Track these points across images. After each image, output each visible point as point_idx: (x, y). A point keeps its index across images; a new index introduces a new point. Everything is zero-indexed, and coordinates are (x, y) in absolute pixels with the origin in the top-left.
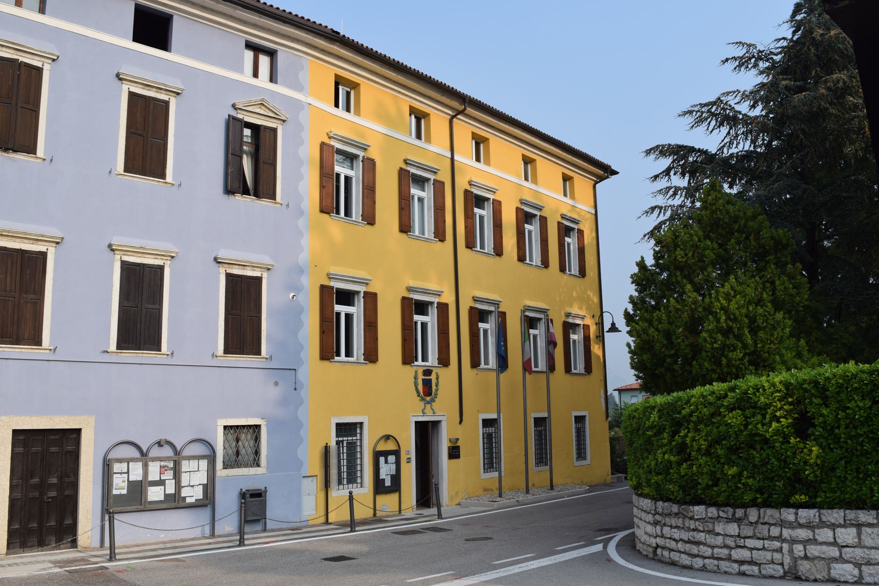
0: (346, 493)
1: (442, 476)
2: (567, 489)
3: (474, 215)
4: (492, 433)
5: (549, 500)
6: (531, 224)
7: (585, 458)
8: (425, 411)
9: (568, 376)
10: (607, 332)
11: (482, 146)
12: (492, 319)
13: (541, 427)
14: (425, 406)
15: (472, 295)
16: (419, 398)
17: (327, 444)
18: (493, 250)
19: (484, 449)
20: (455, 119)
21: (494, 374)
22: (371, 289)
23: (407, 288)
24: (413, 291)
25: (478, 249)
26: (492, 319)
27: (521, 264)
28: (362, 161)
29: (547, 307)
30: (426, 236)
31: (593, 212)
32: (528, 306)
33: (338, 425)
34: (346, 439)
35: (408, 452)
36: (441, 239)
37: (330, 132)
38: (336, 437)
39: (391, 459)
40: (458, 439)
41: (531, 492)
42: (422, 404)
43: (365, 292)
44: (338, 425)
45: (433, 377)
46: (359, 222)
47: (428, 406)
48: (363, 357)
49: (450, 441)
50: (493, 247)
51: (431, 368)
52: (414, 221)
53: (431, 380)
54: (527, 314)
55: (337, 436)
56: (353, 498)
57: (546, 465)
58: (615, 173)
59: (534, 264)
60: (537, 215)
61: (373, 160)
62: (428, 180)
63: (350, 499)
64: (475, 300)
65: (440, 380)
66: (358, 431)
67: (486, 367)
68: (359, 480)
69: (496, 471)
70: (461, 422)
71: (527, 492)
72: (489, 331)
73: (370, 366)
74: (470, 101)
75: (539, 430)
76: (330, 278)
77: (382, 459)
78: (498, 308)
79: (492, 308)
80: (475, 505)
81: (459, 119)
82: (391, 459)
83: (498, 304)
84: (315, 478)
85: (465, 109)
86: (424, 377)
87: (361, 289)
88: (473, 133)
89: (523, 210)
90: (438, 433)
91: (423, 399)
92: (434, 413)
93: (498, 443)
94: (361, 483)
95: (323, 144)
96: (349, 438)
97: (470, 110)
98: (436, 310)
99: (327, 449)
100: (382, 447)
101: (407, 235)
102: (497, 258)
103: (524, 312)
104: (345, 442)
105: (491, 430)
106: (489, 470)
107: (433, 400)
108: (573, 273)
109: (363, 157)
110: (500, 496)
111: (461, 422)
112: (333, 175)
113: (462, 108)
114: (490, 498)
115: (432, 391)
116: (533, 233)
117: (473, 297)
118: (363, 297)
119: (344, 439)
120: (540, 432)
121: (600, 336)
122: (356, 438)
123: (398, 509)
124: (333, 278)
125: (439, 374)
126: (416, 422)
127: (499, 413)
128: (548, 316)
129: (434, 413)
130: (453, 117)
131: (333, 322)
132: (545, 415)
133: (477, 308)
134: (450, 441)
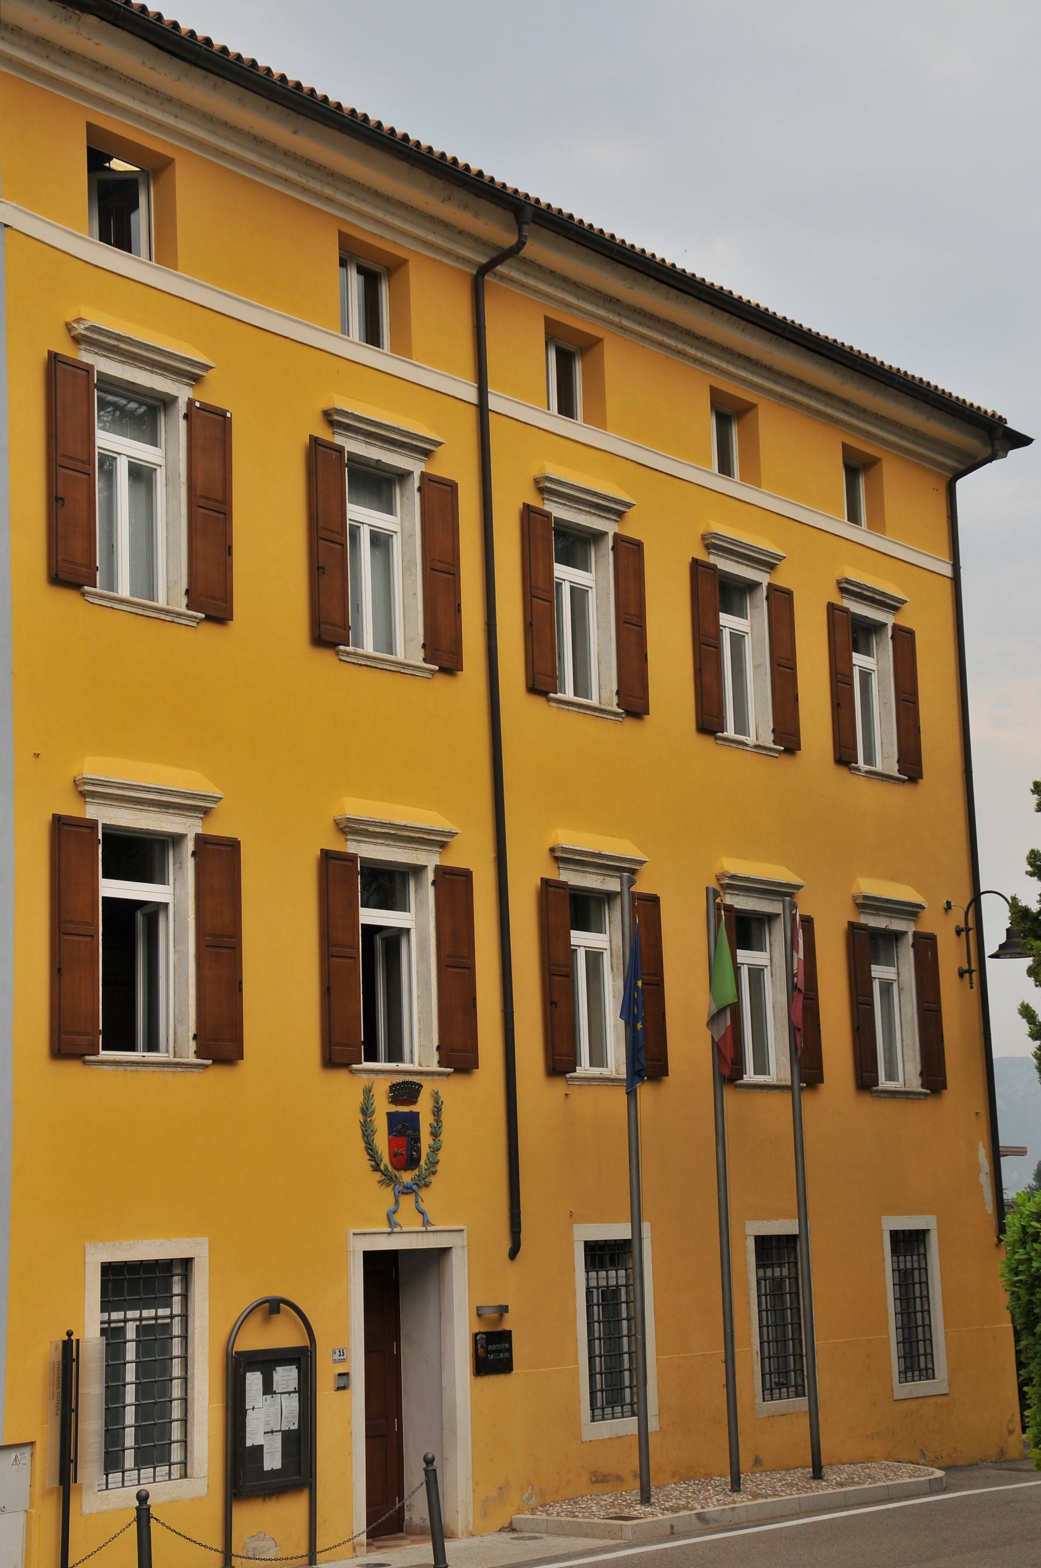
0: (124, 1499)
1: (454, 1432)
2: (870, 1476)
3: (553, 587)
4: (617, 1286)
5: (807, 1514)
6: (741, 613)
7: (928, 1373)
8: (396, 1218)
9: (867, 1100)
10: (991, 956)
11: (578, 367)
12: (615, 919)
13: (780, 1265)
14: (397, 1202)
15: (550, 843)
16: (378, 1176)
17: (70, 1334)
18: (615, 700)
19: (591, 1341)
20: (488, 278)
21: (620, 1095)
22: (219, 828)
23: (337, 823)
24: (356, 832)
25: (569, 694)
26: (615, 919)
27: (707, 742)
28: (186, 416)
29: (795, 880)
30: (400, 656)
31: (947, 570)
32: (733, 877)
33: (108, 1269)
34: (136, 1314)
35: (342, 1355)
36: (446, 665)
37: (79, 320)
38: (103, 1311)
39: (286, 1377)
40: (503, 1310)
41: (747, 1484)
42: (388, 1193)
43: (199, 839)
44: (108, 1269)
45: (423, 1107)
46: (179, 615)
47: (407, 1202)
48: (192, 1046)
49: (479, 1315)
50: (615, 687)
51: (416, 1079)
52: (358, 608)
53: (415, 1117)
54: (729, 900)
55: (105, 1307)
56: (149, 1517)
57: (797, 1395)
58: (1023, 441)
59: (751, 740)
60: (758, 584)
61: (221, 413)
62: (402, 476)
63: (139, 1519)
64: (557, 859)
65: (444, 1117)
66: (177, 1289)
67: (596, 1071)
68: (176, 1455)
69: (633, 1414)
70: (514, 1253)
71: (736, 1486)
72: (606, 956)
73: (218, 1076)
74: (535, 215)
75: (773, 1279)
76: (83, 795)
77: (254, 1380)
78: (632, 883)
79: (613, 885)
80: (562, 1531)
81: (502, 277)
82: (286, 1377)
83: (633, 872)
84: (27, 1451)
85: (521, 244)
86: (393, 1108)
87: (189, 827)
88: (549, 323)
89: (714, 567)
90: (440, 1290)
91: (389, 1179)
92: (426, 1222)
93: (637, 1320)
94: (184, 1463)
95: (54, 360)
96: (146, 1313)
97: (537, 249)
98: (431, 891)
99: (69, 1350)
100: (253, 1340)
101: (337, 653)
102: (630, 724)
103: (716, 894)
104: (131, 1333)
105: (615, 1277)
106: (608, 1410)
107: (422, 1183)
108: (879, 767)
109: (190, 403)
110: (646, 1498)
111: (514, 1253)
112: (90, 462)
113: (509, 240)
114: (613, 1505)
115: (419, 1151)
116: (748, 642)
117: (552, 850)
118: (194, 854)
119: (130, 1314)
120: (778, 1283)
121: (970, 971)
122: (166, 1312)
123: (304, 1550)
124: (93, 794)
125: (443, 1097)
126: (366, 1254)
127: (637, 1229)
128: (794, 906)
129: (426, 1222)
130: (484, 270)
131: (93, 936)
132: (789, 1227)
133: (563, 885)
134: (479, 1313)
